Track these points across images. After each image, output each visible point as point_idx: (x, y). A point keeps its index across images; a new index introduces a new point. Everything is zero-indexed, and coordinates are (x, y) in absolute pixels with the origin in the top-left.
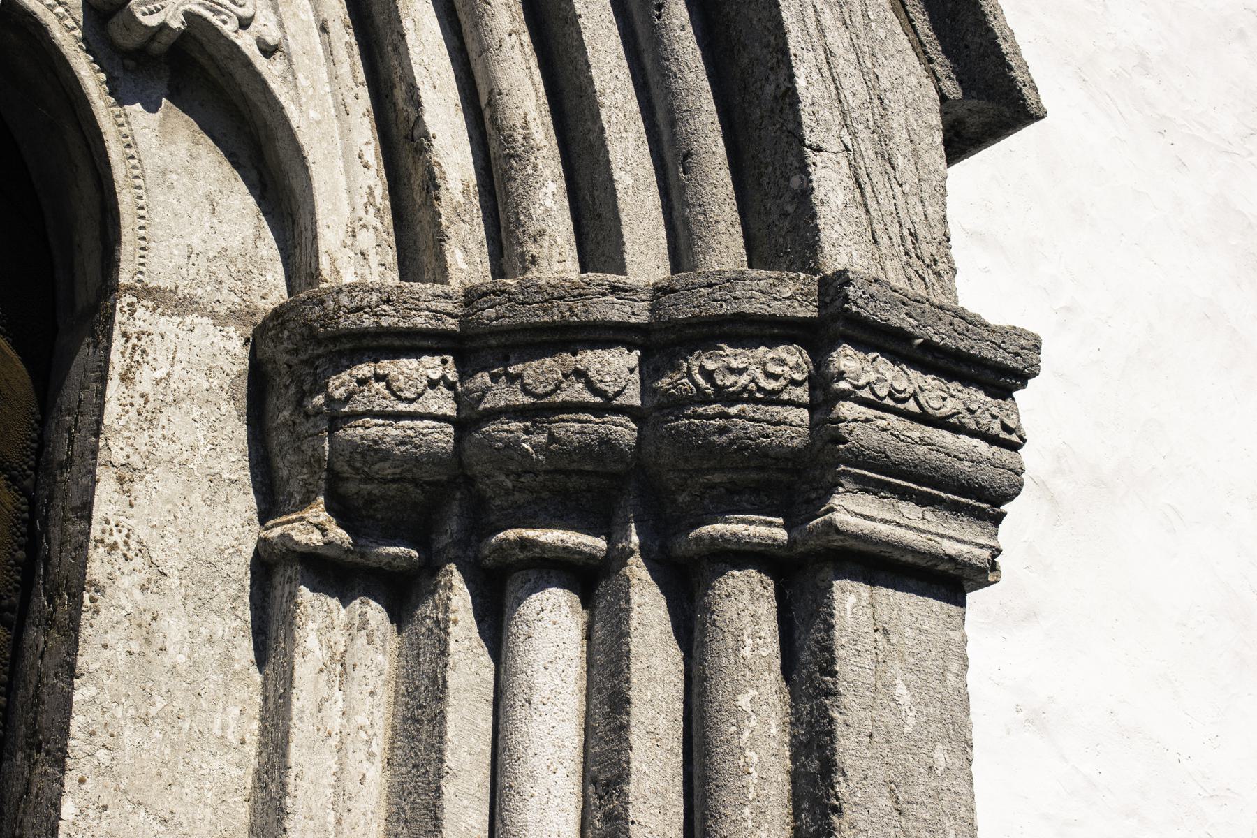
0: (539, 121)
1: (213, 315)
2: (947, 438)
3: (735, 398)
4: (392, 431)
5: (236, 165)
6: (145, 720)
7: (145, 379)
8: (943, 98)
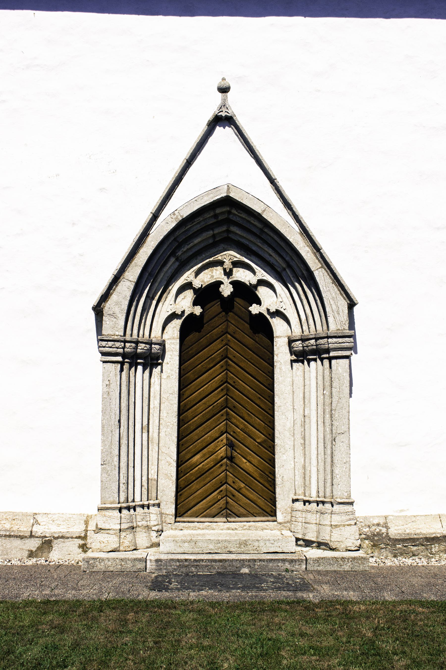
0: (113, 515)
1: (284, 337)
2: (343, 344)
3: (321, 345)
4: (297, 349)
5: (285, 321)
6: (282, 377)
7: (278, 345)
8: (348, 303)
